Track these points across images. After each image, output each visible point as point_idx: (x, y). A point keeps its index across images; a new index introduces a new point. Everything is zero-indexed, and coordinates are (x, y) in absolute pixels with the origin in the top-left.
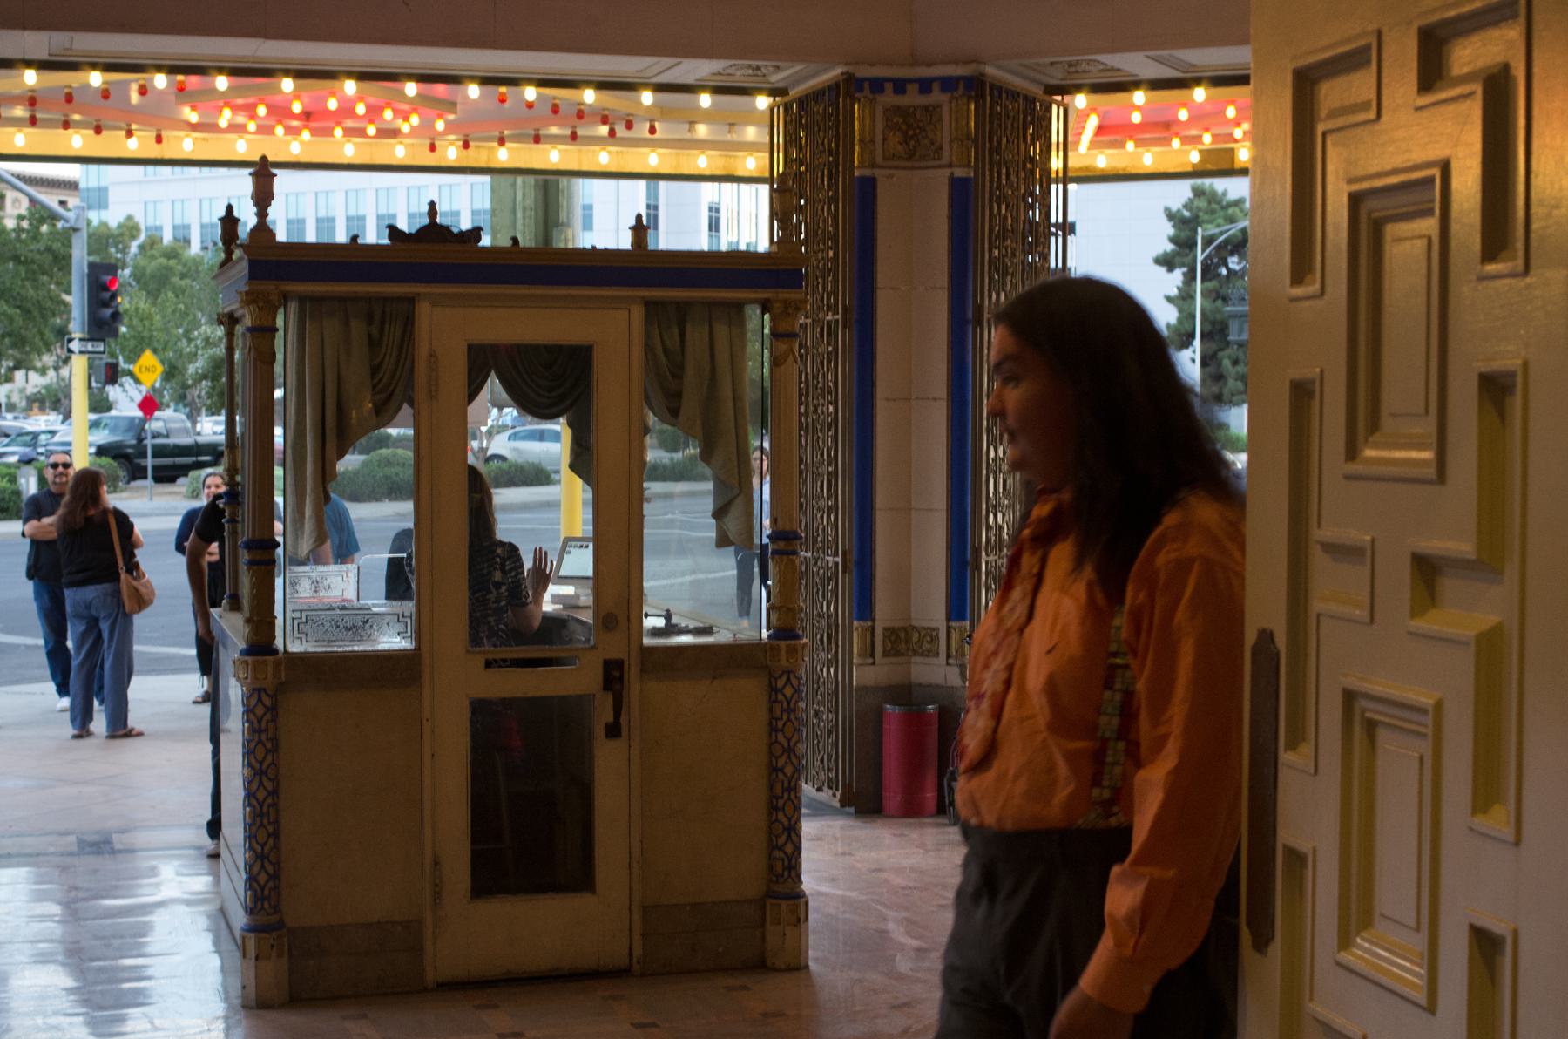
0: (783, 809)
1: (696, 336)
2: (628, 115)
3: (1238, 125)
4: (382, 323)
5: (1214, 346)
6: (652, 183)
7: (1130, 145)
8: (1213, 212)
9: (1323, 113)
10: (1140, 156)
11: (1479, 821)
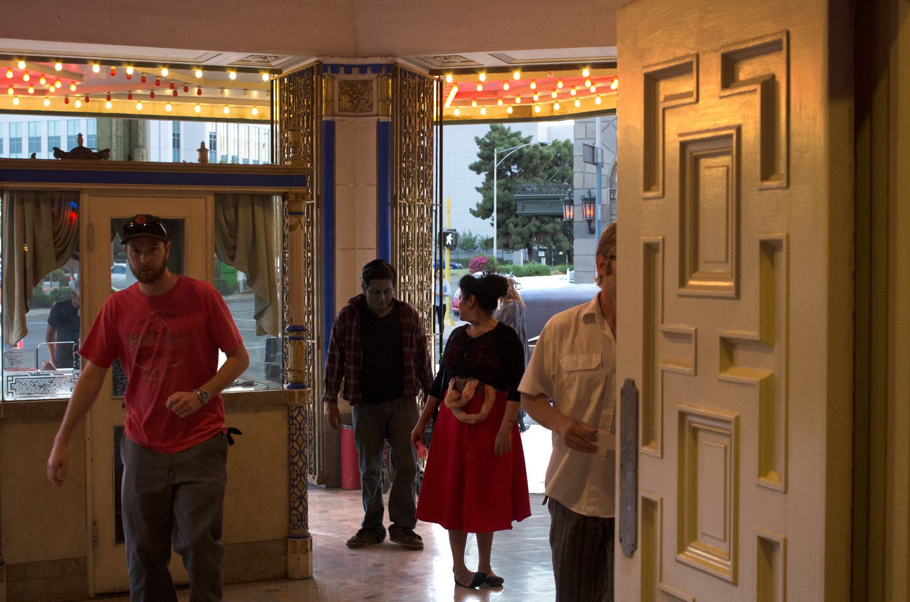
0: (297, 486)
1: (244, 214)
2: (186, 83)
3: (536, 93)
4: (60, 206)
5: (504, 216)
6: (176, 122)
7: (474, 104)
8: (502, 140)
9: (662, 98)
10: (479, 110)
11: (763, 480)
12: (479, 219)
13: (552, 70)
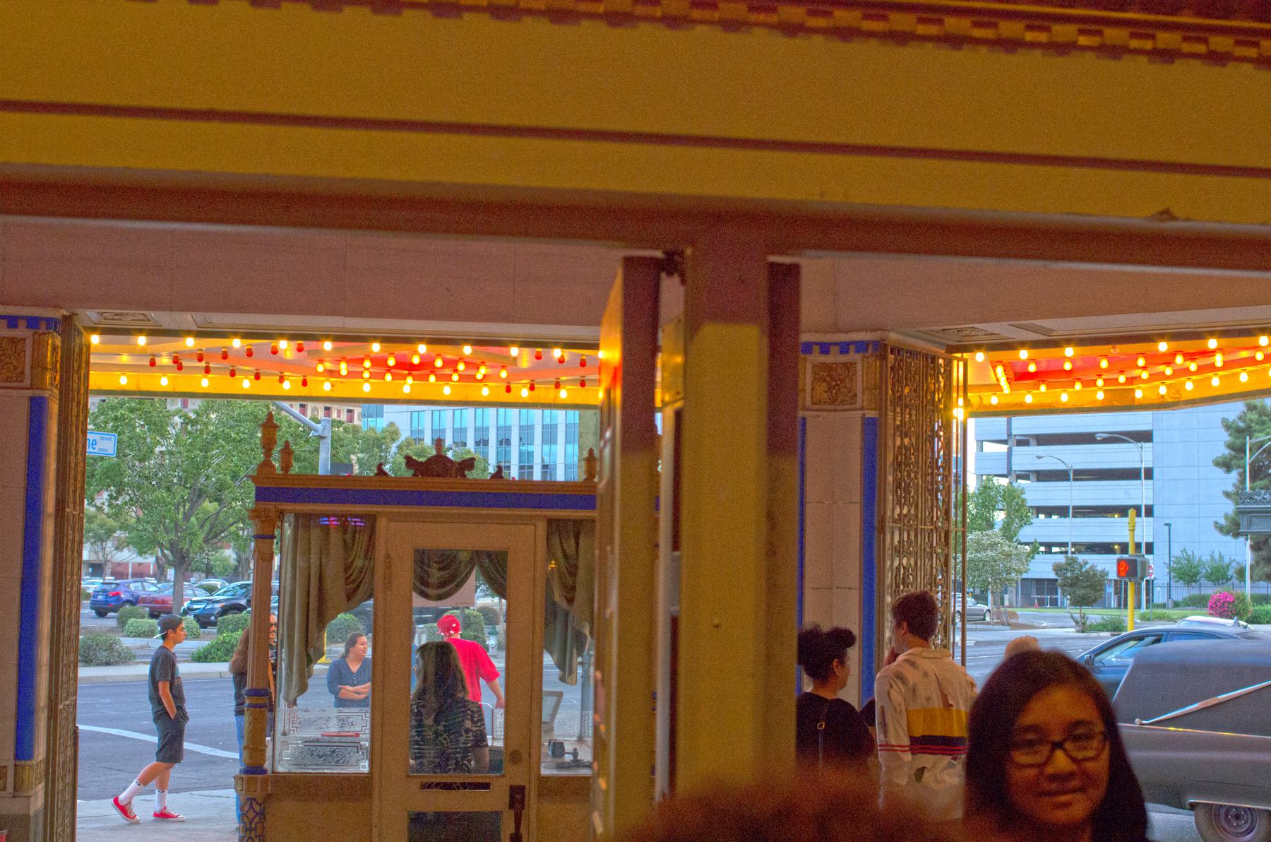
8: (1263, 423)
12: (1229, 538)
13: (1117, 343)
